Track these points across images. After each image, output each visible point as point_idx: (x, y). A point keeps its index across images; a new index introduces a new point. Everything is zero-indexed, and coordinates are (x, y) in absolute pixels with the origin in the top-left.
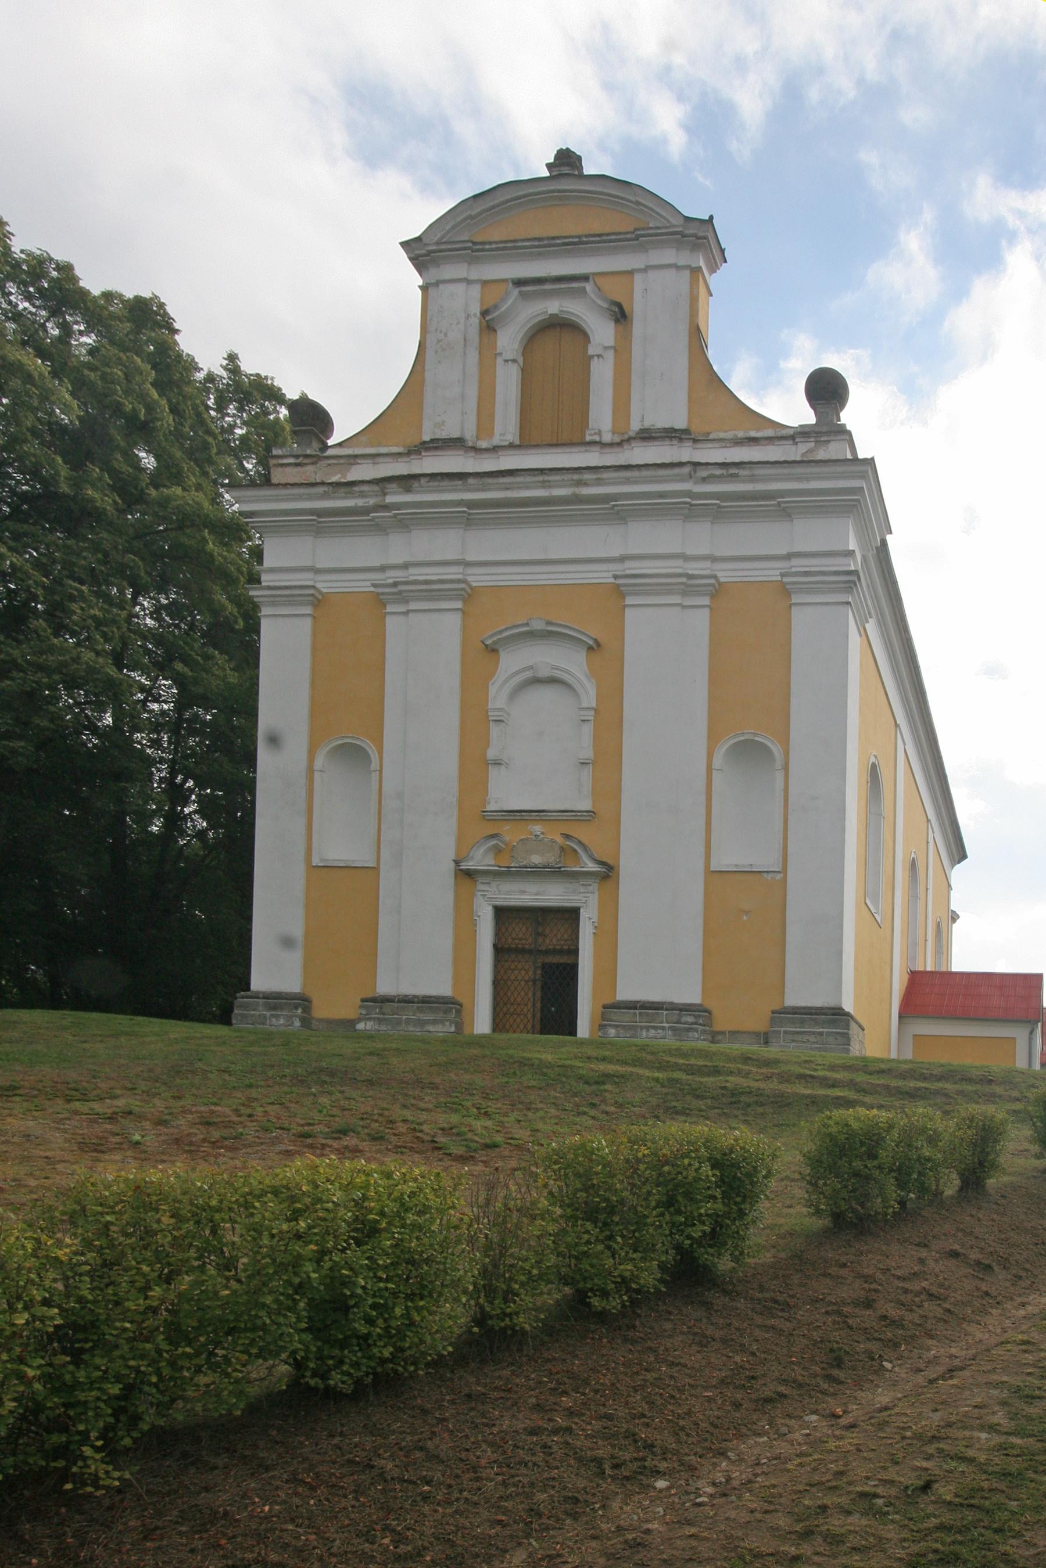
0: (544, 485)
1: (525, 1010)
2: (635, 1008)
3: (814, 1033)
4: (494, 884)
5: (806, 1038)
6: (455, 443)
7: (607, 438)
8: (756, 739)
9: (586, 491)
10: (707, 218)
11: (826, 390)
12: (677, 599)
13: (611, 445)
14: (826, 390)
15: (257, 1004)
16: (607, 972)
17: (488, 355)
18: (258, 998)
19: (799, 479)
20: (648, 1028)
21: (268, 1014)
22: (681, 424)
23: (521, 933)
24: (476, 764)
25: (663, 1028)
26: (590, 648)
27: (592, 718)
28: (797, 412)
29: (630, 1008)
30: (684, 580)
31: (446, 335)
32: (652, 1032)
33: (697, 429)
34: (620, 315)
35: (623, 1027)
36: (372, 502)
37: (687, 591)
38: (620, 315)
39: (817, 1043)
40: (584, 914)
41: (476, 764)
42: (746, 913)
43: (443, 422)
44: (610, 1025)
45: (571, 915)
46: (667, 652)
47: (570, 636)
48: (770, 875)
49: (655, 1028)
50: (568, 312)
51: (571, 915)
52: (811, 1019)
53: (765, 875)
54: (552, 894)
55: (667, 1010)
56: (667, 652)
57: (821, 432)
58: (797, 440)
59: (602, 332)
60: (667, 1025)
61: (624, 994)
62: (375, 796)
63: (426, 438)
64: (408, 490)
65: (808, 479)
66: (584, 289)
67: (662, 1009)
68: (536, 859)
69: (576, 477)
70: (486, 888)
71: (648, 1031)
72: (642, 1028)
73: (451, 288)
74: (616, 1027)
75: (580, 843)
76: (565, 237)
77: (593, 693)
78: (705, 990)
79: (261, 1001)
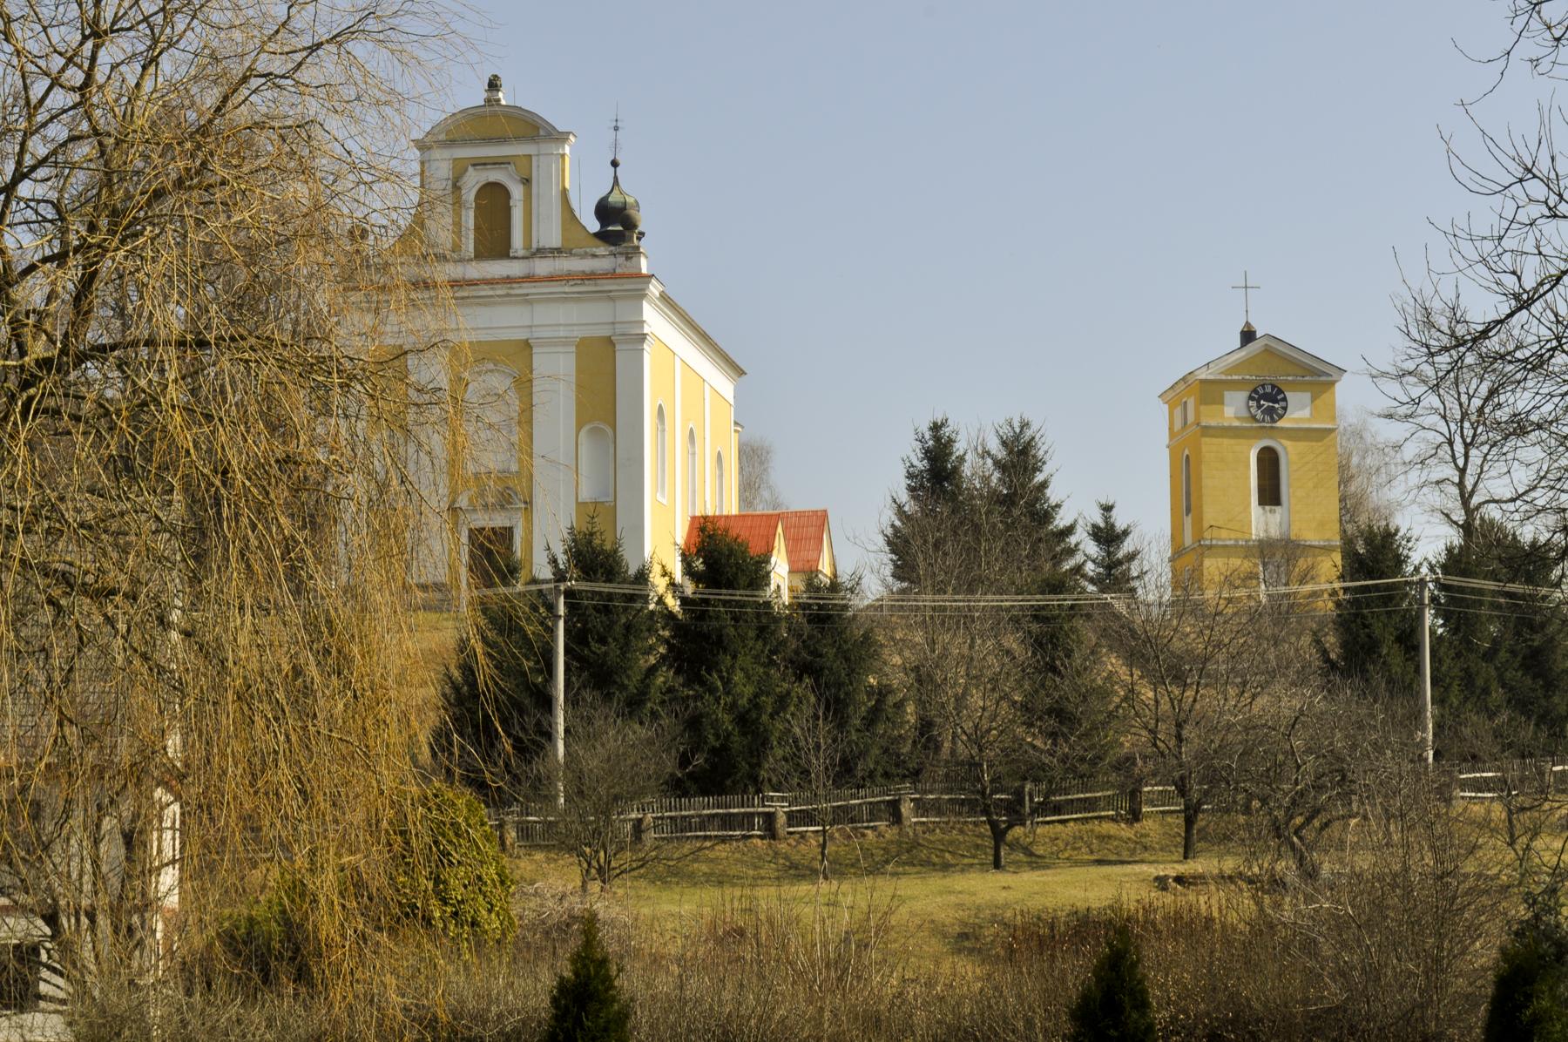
7: (521, 253)
12: (561, 349)
34: (527, 182)
37: (565, 344)
38: (527, 182)
51: (510, 530)
54: (499, 520)
56: (556, 373)
59: (517, 192)
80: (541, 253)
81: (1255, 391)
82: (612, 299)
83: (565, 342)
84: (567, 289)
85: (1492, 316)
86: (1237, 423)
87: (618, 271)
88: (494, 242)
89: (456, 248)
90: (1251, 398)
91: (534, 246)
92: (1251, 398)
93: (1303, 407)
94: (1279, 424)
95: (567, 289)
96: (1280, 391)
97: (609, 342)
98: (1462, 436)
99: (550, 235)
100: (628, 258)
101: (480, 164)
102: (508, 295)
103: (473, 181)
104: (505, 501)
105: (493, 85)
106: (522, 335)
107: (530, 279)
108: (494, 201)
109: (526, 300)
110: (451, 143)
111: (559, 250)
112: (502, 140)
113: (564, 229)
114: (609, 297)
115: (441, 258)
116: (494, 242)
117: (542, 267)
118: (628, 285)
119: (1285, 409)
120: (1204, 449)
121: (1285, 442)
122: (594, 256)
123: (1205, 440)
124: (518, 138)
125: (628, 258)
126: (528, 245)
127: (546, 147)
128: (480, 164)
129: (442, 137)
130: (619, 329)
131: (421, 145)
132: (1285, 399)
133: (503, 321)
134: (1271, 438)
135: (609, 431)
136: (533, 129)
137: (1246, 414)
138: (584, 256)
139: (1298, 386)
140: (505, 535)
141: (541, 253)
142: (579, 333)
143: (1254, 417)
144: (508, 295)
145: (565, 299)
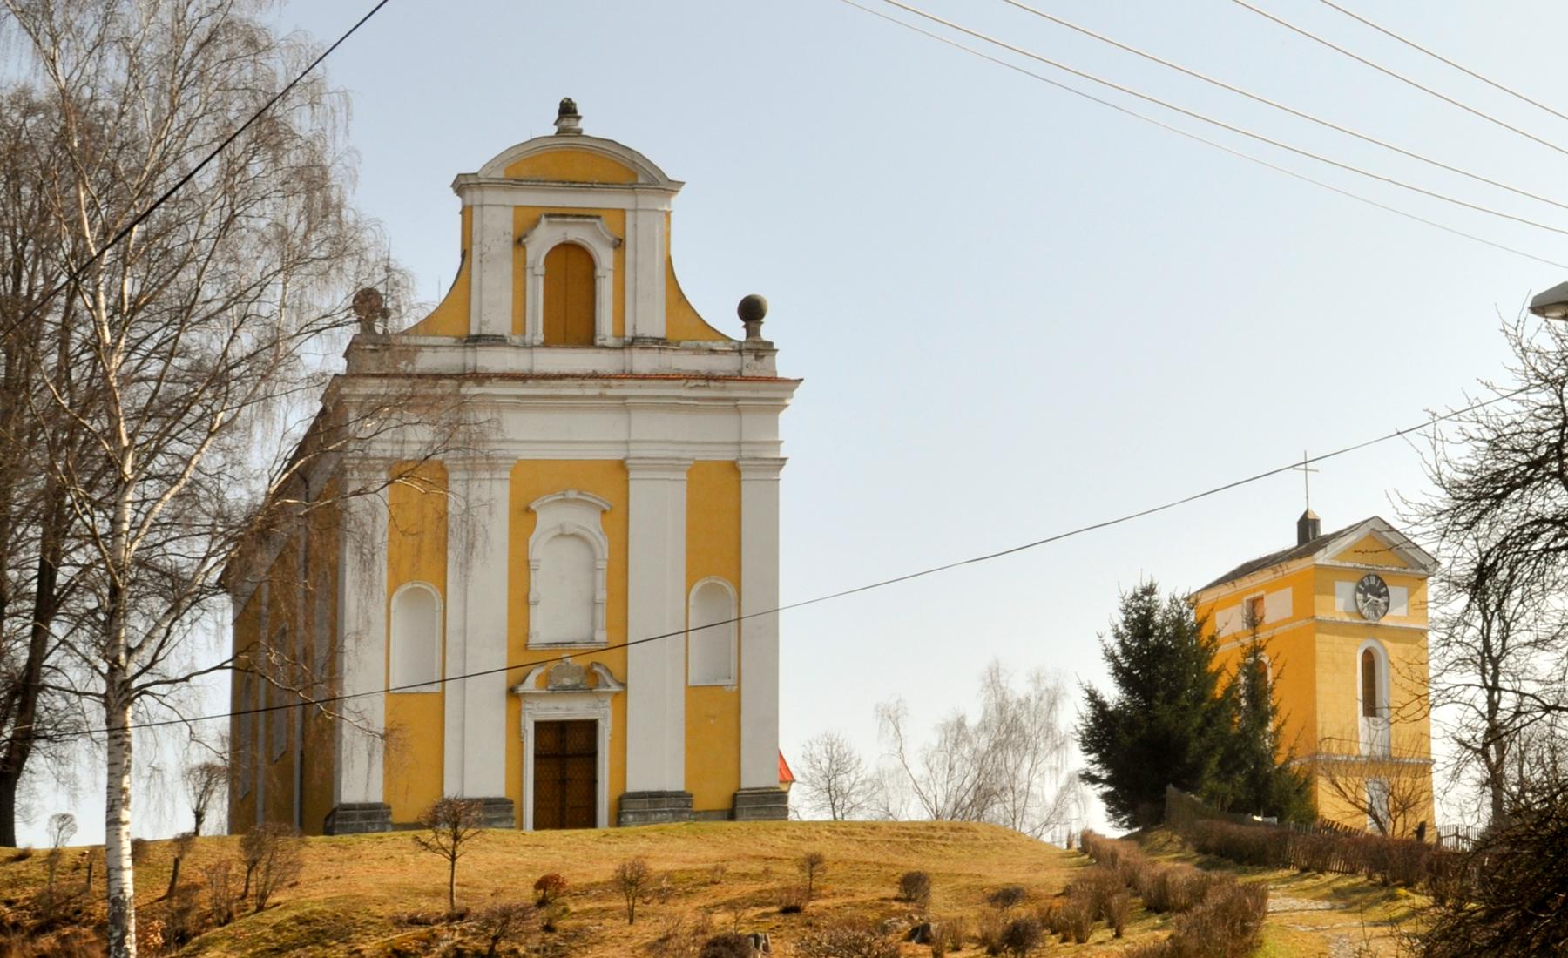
0: (581, 386)
6: (498, 341)
7: (610, 342)
10: (1290, 540)
11: (751, 311)
12: (667, 475)
13: (615, 348)
14: (751, 311)
16: (621, 771)
17: (521, 270)
19: (753, 390)
23: (575, 742)
24: (521, 602)
26: (604, 512)
28: (735, 329)
34: (619, 244)
36: (595, 392)
37: (676, 468)
38: (619, 244)
40: (601, 723)
41: (521, 602)
45: (591, 727)
51: (591, 727)
54: (574, 709)
56: (660, 513)
59: (605, 258)
62: (439, 630)
63: (474, 332)
68: (567, 681)
73: (494, 210)
75: (607, 670)
77: (606, 548)
80: (636, 342)
81: (1362, 582)
82: (738, 410)
83: (673, 465)
84: (684, 393)
86: (1347, 619)
87: (746, 373)
88: (572, 319)
89: (520, 325)
90: (1358, 590)
91: (629, 333)
92: (1358, 590)
93: (1401, 604)
94: (1384, 621)
95: (684, 393)
96: (1383, 584)
97: (734, 468)
98: (157, 683)
100: (758, 357)
101: (558, 215)
102: (601, 396)
103: (545, 238)
104: (589, 682)
105: (567, 110)
107: (628, 376)
109: (624, 405)
110: (514, 182)
111: (657, 340)
112: (586, 185)
113: (669, 314)
114: (736, 406)
115: (498, 341)
116: (572, 319)
117: (643, 361)
118: (765, 391)
119: (1387, 604)
120: (1318, 647)
121: (1388, 644)
122: (712, 351)
123: (1319, 637)
125: (758, 357)
126: (620, 334)
127: (646, 201)
128: (558, 215)
129: (501, 174)
130: (747, 451)
131: (462, 185)
132: (1387, 594)
133: (585, 434)
134: (1374, 638)
135: (731, 590)
136: (633, 175)
137: (1353, 609)
138: (697, 350)
139: (1400, 578)
140: (589, 728)
141: (636, 342)
142: (701, 454)
143: (1359, 613)
144: (601, 396)
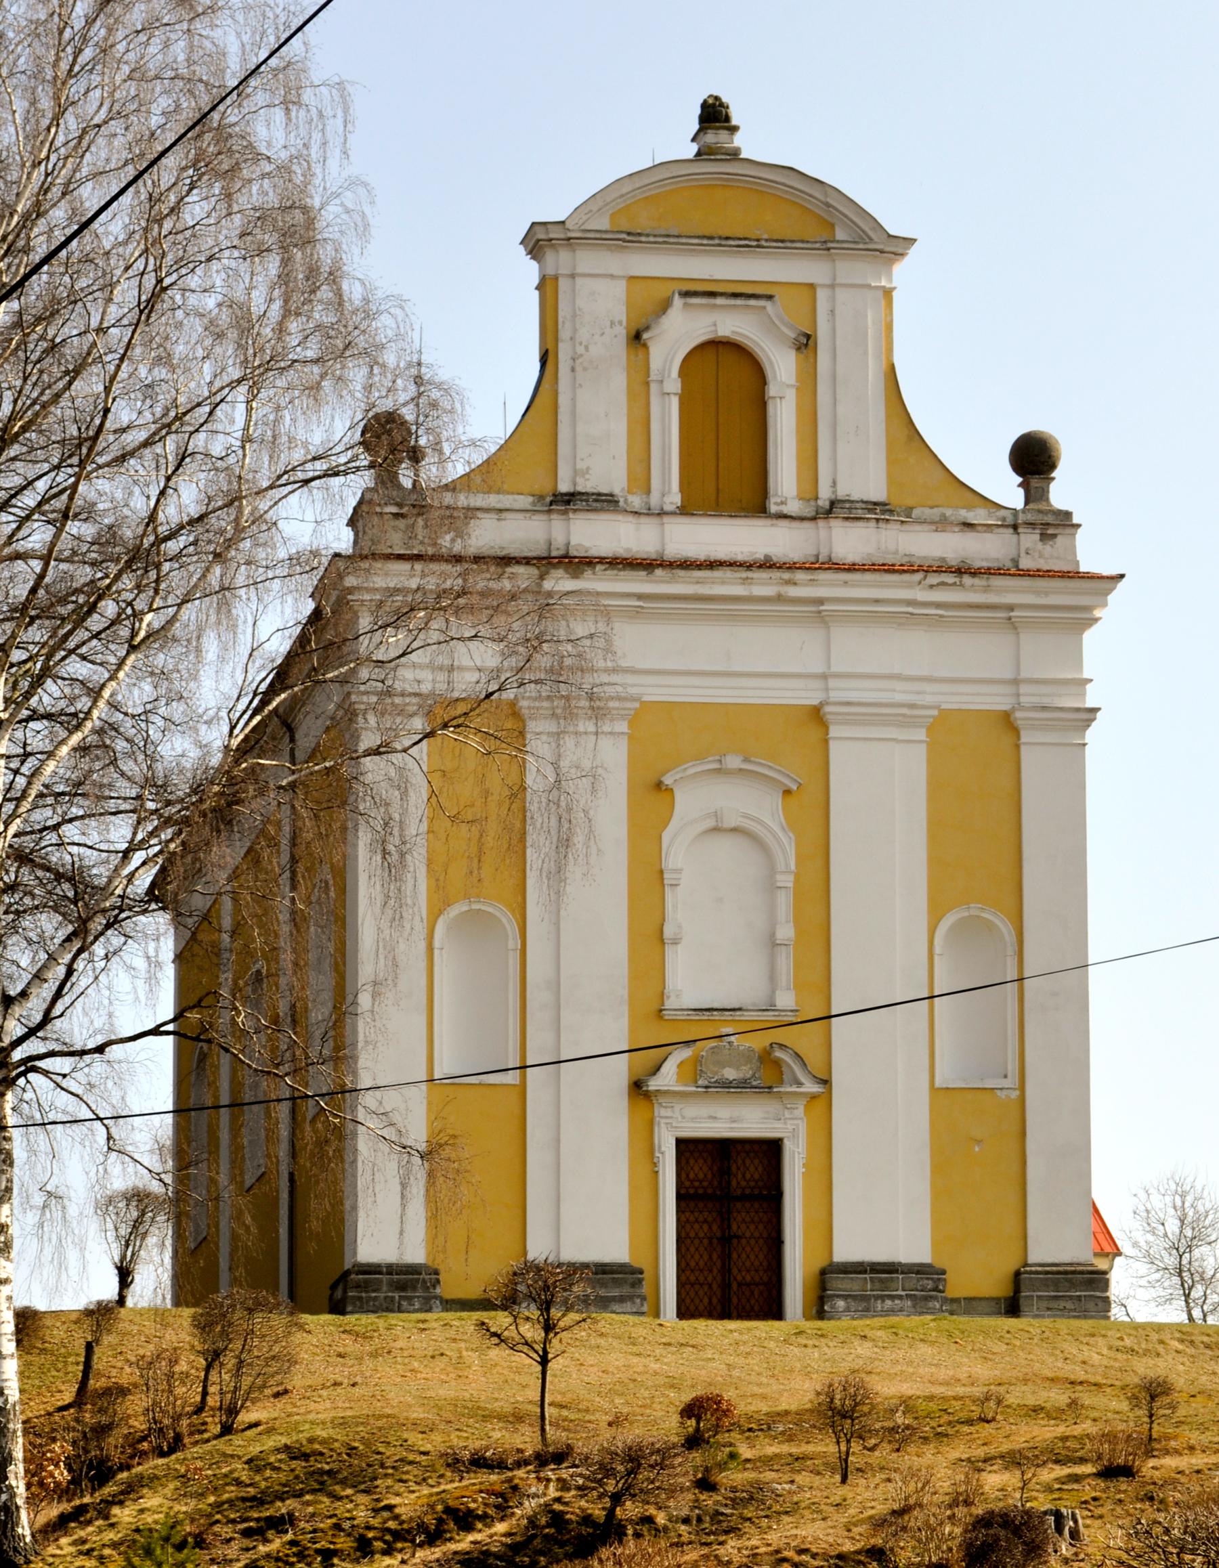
1: (710, 1278)
2: (865, 1272)
3: (1071, 1297)
4: (677, 1107)
5: (1062, 1304)
6: (604, 502)
7: (793, 507)
8: (984, 915)
9: (793, 592)
11: (1033, 458)
15: (381, 1281)
17: (641, 384)
18: (380, 1273)
20: (883, 1298)
21: (396, 1295)
22: (877, 492)
25: (900, 1297)
26: (787, 792)
27: (791, 885)
28: (1007, 490)
29: (860, 1273)
30: (905, 711)
31: (587, 348)
32: (889, 1303)
33: (895, 502)
34: (805, 343)
35: (854, 1297)
38: (805, 343)
39: (1075, 1310)
42: (979, 1142)
43: (588, 469)
44: (838, 1296)
45: (771, 1150)
46: (881, 797)
47: (757, 773)
48: (1005, 1092)
49: (892, 1298)
50: (761, 348)
51: (771, 1150)
52: (1066, 1280)
53: (998, 1092)
55: (902, 1273)
56: (881, 797)
57: (1048, 524)
58: (1020, 530)
59: (782, 367)
60: (903, 1293)
61: (844, 1253)
64: (576, 576)
65: (1047, 594)
66: (764, 308)
67: (896, 1272)
68: (730, 1074)
69: (787, 575)
70: (668, 1113)
71: (883, 1301)
72: (877, 1298)
74: (845, 1297)
76: (740, 239)
78: (935, 1244)
79: (385, 1278)
80: (834, 509)
83: (903, 716)
85: (615, 273)
87: (1025, 563)
89: (641, 478)
91: (825, 494)
99: (862, 472)
100: (1045, 537)
101: (701, 293)
103: (680, 332)
104: (766, 1076)
105: (714, 115)
106: (809, 696)
108: (727, 386)
109: (818, 613)
110: (628, 238)
111: (873, 506)
113: (892, 462)
114: (1009, 619)
117: (850, 541)
118: (1059, 594)
122: (968, 526)
124: (782, 243)
125: (1045, 537)
127: (851, 270)
128: (701, 293)
138: (941, 524)
141: (834, 509)
144: (780, 599)
145: (909, 617)
